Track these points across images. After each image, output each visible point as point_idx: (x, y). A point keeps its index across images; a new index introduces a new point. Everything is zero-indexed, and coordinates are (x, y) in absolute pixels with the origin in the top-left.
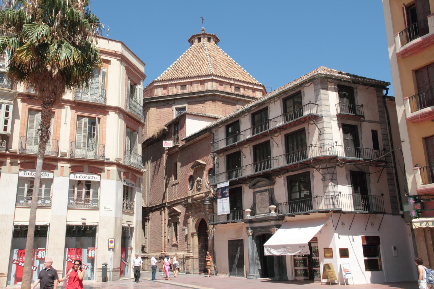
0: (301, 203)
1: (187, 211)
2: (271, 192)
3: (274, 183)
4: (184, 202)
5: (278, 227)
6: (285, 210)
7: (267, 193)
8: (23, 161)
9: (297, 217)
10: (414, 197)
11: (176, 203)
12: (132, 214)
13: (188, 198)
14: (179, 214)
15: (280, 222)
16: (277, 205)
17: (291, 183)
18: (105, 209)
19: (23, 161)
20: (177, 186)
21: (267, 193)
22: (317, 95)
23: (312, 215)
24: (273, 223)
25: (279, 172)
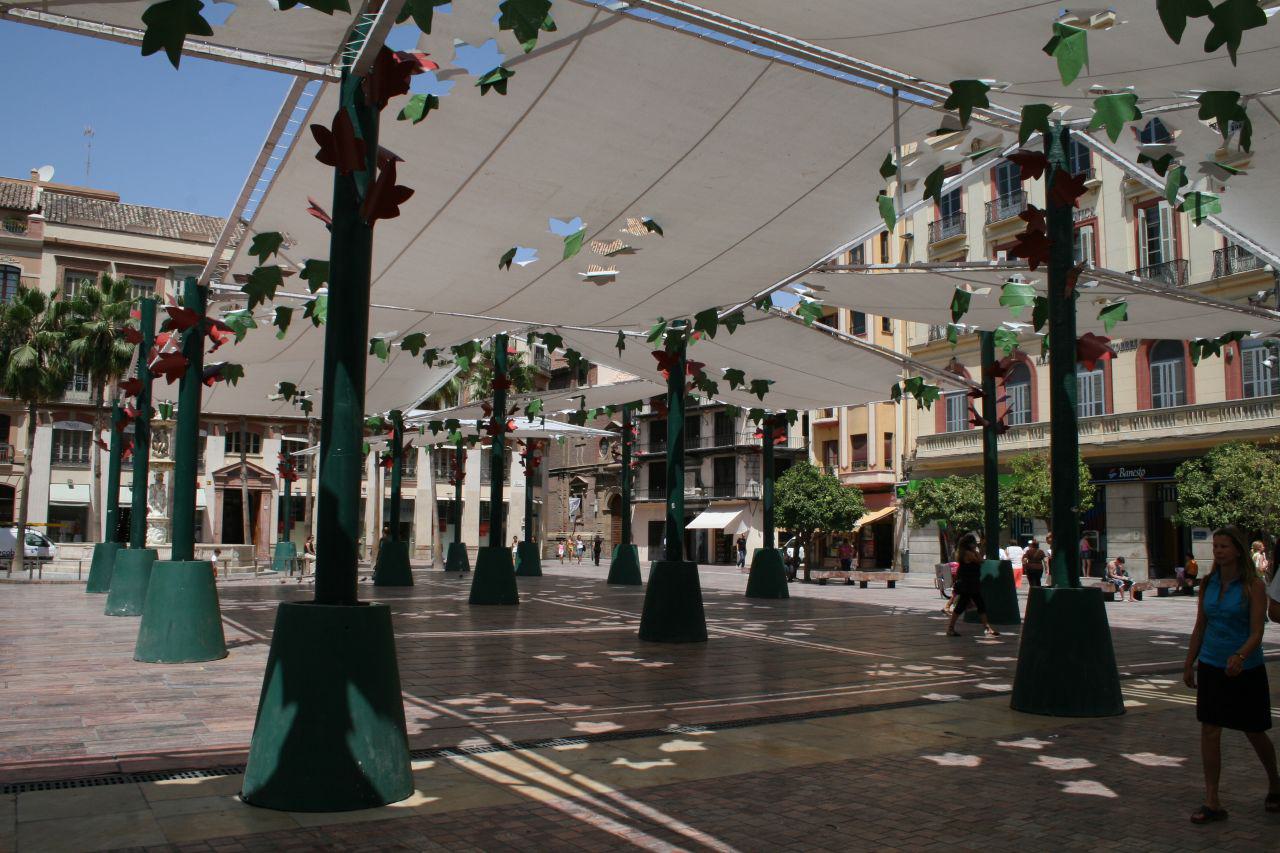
0: (725, 485)
1: (597, 482)
2: (698, 473)
3: (701, 463)
4: (593, 471)
5: (702, 510)
6: (709, 495)
7: (694, 474)
8: (55, 411)
9: (721, 502)
10: (1175, 577)
11: (585, 471)
12: (110, 263)
13: (599, 465)
14: (586, 485)
15: (703, 506)
16: (703, 488)
17: (717, 464)
18: (516, 486)
19: (55, 411)
20: (582, 448)
21: (694, 474)
22: (1002, 361)
23: (735, 501)
24: (697, 506)
25: (708, 453)
